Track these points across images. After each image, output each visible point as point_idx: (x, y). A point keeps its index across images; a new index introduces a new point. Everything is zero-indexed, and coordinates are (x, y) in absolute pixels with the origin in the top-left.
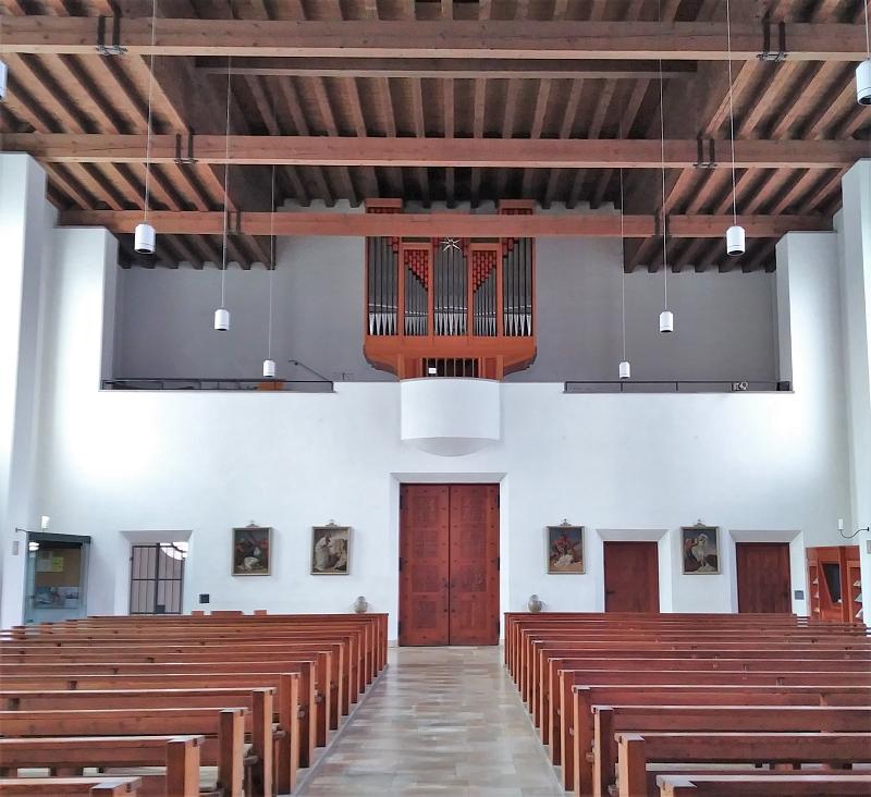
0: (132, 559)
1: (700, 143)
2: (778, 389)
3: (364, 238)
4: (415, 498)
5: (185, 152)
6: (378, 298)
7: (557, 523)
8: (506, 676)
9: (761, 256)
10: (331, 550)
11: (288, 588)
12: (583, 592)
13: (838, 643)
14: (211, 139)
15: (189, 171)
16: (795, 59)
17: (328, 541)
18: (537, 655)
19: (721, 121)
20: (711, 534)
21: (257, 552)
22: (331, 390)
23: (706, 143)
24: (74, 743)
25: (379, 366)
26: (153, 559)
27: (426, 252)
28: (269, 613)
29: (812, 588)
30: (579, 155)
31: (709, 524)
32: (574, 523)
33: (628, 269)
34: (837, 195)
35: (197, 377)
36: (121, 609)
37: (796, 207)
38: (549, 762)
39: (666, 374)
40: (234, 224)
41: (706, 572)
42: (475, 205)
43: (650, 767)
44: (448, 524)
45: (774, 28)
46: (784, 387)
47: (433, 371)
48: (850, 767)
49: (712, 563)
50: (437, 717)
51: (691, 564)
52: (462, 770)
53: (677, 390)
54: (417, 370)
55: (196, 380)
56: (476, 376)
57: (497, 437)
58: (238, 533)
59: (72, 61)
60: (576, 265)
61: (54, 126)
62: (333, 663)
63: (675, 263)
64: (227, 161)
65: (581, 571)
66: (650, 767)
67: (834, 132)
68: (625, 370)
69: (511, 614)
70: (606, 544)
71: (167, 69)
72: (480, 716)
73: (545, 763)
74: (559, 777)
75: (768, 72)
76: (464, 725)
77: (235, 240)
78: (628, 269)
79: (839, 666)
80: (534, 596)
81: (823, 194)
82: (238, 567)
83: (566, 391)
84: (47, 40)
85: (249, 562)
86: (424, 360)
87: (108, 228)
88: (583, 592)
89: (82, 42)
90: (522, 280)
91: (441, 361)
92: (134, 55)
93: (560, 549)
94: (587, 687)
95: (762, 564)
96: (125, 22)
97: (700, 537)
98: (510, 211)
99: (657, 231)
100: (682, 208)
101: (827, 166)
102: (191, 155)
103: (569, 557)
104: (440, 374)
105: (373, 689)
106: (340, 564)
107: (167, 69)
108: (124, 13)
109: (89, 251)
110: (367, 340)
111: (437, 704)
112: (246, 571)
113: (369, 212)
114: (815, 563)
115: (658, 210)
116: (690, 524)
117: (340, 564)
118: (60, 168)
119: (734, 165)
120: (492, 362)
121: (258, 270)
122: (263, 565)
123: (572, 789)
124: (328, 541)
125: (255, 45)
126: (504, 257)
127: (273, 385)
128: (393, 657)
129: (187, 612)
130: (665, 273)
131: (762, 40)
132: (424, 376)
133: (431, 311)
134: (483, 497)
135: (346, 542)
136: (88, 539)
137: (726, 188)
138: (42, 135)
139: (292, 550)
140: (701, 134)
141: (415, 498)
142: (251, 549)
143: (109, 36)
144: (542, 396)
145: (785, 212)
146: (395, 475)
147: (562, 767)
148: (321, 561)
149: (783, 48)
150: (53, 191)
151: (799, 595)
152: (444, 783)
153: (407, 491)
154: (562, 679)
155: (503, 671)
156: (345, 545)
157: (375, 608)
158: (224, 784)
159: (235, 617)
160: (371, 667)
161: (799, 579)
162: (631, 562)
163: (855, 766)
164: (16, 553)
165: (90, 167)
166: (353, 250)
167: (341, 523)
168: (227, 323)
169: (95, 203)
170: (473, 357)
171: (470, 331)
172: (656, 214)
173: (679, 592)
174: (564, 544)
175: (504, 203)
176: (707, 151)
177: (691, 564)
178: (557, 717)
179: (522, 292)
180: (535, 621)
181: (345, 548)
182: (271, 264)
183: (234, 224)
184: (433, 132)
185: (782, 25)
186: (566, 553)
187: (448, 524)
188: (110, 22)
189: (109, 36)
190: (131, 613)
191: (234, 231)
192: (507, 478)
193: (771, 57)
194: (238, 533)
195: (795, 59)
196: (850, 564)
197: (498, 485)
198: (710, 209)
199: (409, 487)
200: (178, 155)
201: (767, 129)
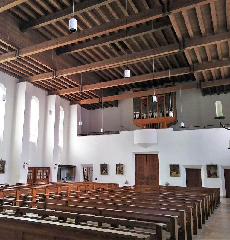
3: (132, 98)
4: (138, 157)
7: (172, 164)
10: (120, 169)
11: (112, 178)
12: (180, 181)
17: (119, 167)
20: (215, 166)
21: (105, 169)
22: (119, 133)
24: (112, 217)
27: (147, 99)
30: (160, 76)
31: (214, 164)
32: (177, 164)
40: (100, 100)
47: (145, 127)
49: (216, 175)
51: (209, 175)
53: (204, 128)
55: (96, 133)
56: (160, 128)
57: (156, 143)
58: (102, 165)
65: (179, 176)
68: (182, 124)
78: (204, 95)
80: (167, 182)
82: (102, 173)
85: (104, 171)
86: (147, 124)
88: (180, 181)
97: (212, 167)
102: (82, 90)
103: (175, 172)
104: (147, 128)
106: (122, 172)
112: (103, 173)
113: (134, 92)
116: (209, 164)
117: (122, 172)
120: (163, 123)
122: (107, 172)
124: (119, 167)
125: (77, 71)
129: (93, 182)
133: (165, 110)
134: (154, 157)
135: (123, 168)
136: (75, 166)
139: (112, 169)
141: (138, 157)
142: (104, 169)
146: (133, 152)
148: (118, 172)
153: (137, 156)
156: (123, 168)
158: (173, 237)
162: (193, 175)
168: (81, 124)
170: (158, 123)
174: (174, 169)
175: (166, 84)
177: (209, 175)
181: (123, 169)
182: (117, 106)
183: (100, 100)
186: (175, 171)
189: (54, 75)
191: (100, 101)
192: (159, 153)
194: (102, 165)
197: (158, 154)
199: (137, 155)
200: (80, 91)
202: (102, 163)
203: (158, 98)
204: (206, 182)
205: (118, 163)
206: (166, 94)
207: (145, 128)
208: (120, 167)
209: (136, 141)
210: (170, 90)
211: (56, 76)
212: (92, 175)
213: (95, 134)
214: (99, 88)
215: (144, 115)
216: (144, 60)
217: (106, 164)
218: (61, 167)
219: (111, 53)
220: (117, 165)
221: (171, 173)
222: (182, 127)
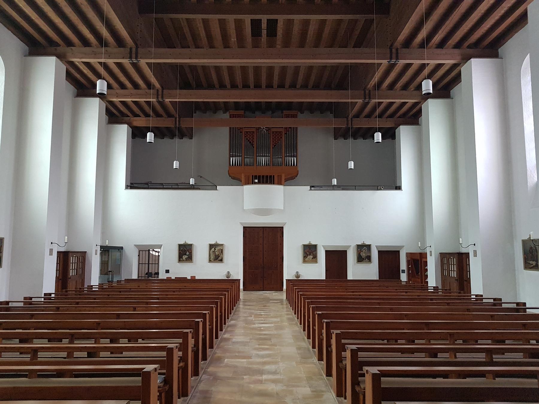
0: (139, 255)
1: (365, 92)
2: (396, 189)
4: (250, 233)
5: (160, 97)
6: (234, 150)
7: (306, 243)
8: (287, 304)
9: (390, 135)
10: (216, 254)
11: (202, 269)
12: (317, 271)
13: (416, 293)
14: (170, 91)
15: (136, 66)
16: (402, 62)
17: (215, 249)
18: (301, 299)
19: (373, 83)
20: (369, 247)
21: (188, 253)
23: (367, 92)
25: (234, 178)
26: (147, 255)
27: (253, 132)
28: (196, 278)
29: (409, 269)
31: (367, 243)
33: (336, 138)
34: (420, 112)
35: (162, 182)
36: (135, 276)
37: (405, 114)
38: (306, 338)
39: (350, 183)
41: (366, 262)
42: (273, 113)
43: (343, 341)
44: (263, 245)
45: (367, 92)
46: (399, 188)
47: (256, 181)
48: (414, 342)
50: (262, 320)
51: (360, 259)
52: (274, 341)
53: (355, 189)
54: (250, 181)
55: (147, 184)
56: (274, 184)
58: (180, 246)
59: (119, 65)
60: (313, 143)
61: (69, 43)
62: (218, 299)
63: (355, 137)
64: (178, 100)
65: (316, 262)
66: (343, 341)
67: (458, 46)
68: (335, 182)
69: (289, 280)
70: (326, 251)
71: (156, 68)
72: (279, 319)
73: (304, 339)
74: (310, 344)
75: (391, 67)
76: (272, 323)
77: (179, 129)
78: (336, 138)
79: (414, 304)
80: (297, 272)
81: (415, 110)
82: (180, 259)
83: (311, 190)
84: (110, 57)
85: (185, 257)
86: (253, 176)
87: (127, 124)
88: (317, 271)
89: (123, 58)
90: (292, 143)
91: (259, 176)
92: (143, 63)
93: (308, 253)
94: (320, 313)
95: (389, 258)
96: (140, 50)
98: (287, 116)
99: (348, 124)
100: (357, 116)
101: (452, 62)
102: (162, 98)
103: (311, 257)
104: (259, 183)
105: (236, 309)
106: (220, 258)
107: (156, 68)
108: (139, 45)
109: (122, 133)
110: (229, 168)
111: (262, 315)
114: (410, 259)
115: (348, 116)
116: (360, 244)
117: (220, 258)
118: (72, 64)
119: (377, 101)
121: (185, 140)
122: (190, 259)
123: (444, 257)
124: (215, 249)
126: (285, 134)
127: (192, 187)
128: (242, 295)
130: (351, 140)
131: (389, 55)
132: (253, 184)
135: (222, 250)
137: (374, 109)
138: (63, 48)
139: (201, 253)
140: (365, 88)
141: (250, 233)
142: (185, 252)
143: (134, 56)
144: (301, 192)
145: (399, 117)
147: (311, 340)
148: (212, 257)
149: (397, 58)
150: (69, 76)
151: (403, 271)
152: (268, 345)
154: (325, 324)
155: (285, 302)
157: (234, 277)
159: (183, 280)
160: (236, 299)
161: (403, 265)
162: (336, 259)
163: (416, 341)
164: (96, 254)
165: (88, 64)
166: (225, 132)
167: (220, 242)
169: (123, 114)
170: (272, 175)
171: (271, 164)
172: (347, 118)
173: (355, 271)
174: (310, 252)
175: (286, 112)
176: (368, 95)
177: (360, 259)
178: (309, 322)
179: (292, 148)
180: (297, 283)
181: (222, 252)
184: (258, 86)
185: (397, 50)
187: (263, 245)
188: (134, 50)
190: (138, 277)
193: (393, 61)
194: (180, 246)
195: (402, 62)
196: (424, 260)
198: (369, 116)
201: (391, 86)
202: (182, 243)
203: (146, 136)
204: (355, 271)
205: (213, 243)
206: (286, 128)
207: (255, 183)
208: (217, 249)
209: (247, 206)
210: (287, 123)
211: (136, 58)
212: (158, 264)
213: (146, 186)
214: (201, 100)
215: (247, 160)
216: (243, 65)
217: (190, 243)
218: (444, 257)
219: (209, 36)
220: (211, 246)
221: (305, 257)
222: (334, 185)
